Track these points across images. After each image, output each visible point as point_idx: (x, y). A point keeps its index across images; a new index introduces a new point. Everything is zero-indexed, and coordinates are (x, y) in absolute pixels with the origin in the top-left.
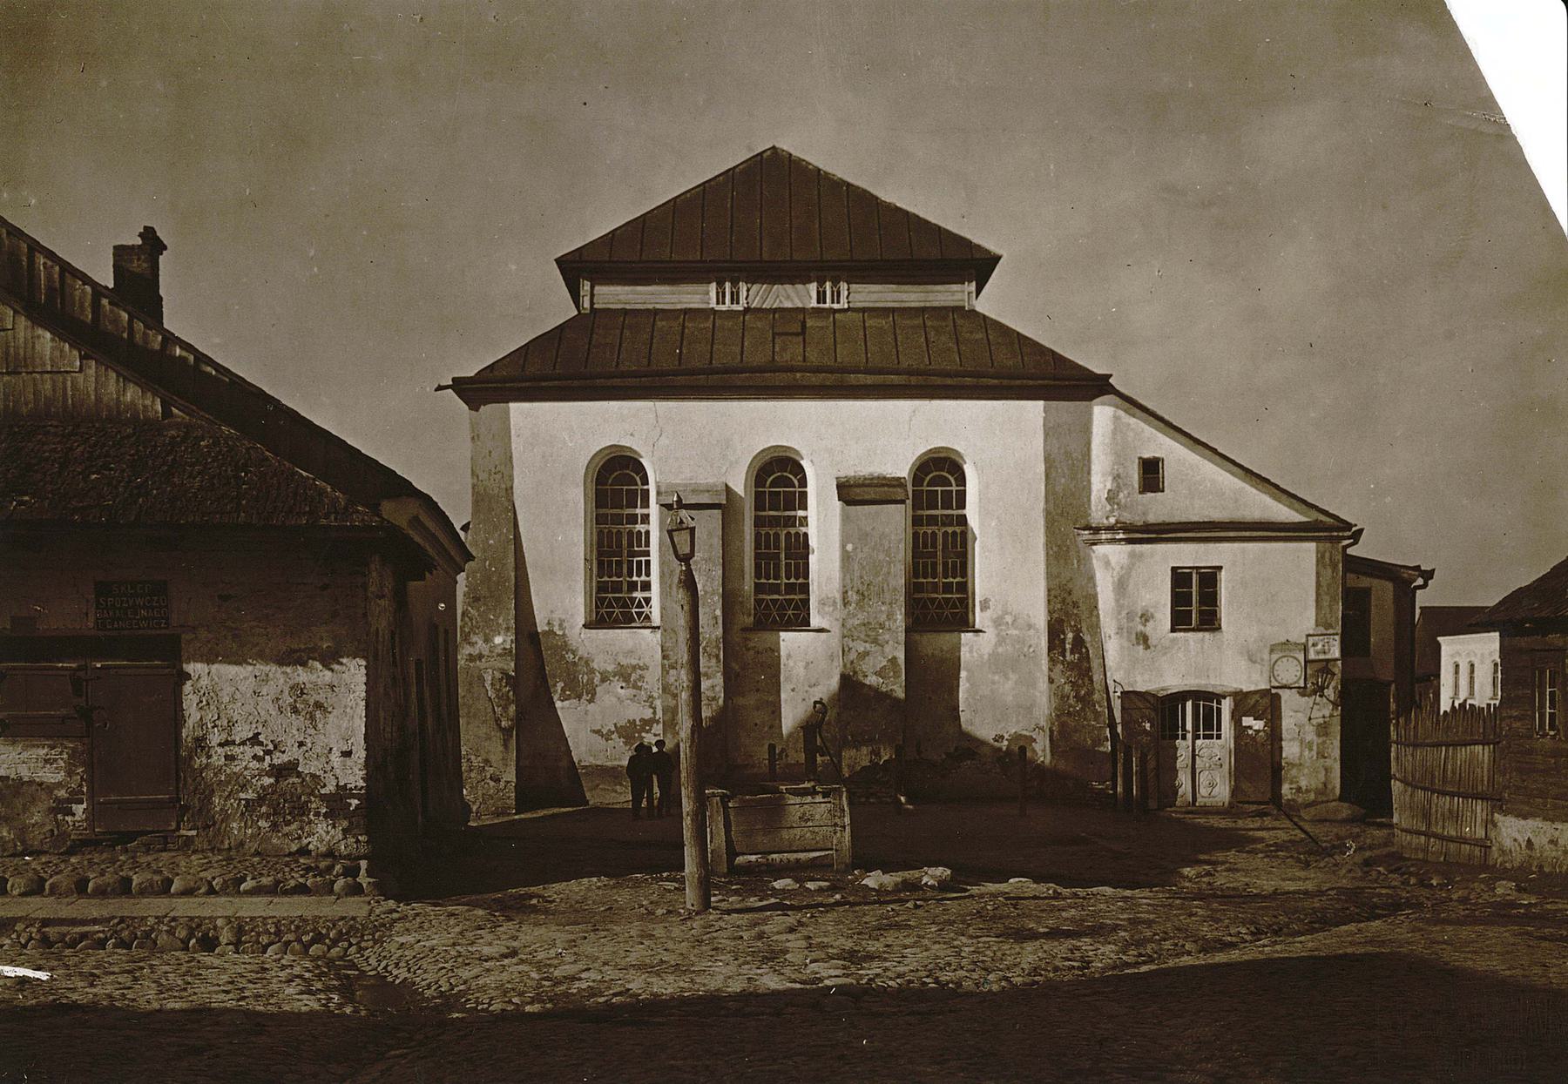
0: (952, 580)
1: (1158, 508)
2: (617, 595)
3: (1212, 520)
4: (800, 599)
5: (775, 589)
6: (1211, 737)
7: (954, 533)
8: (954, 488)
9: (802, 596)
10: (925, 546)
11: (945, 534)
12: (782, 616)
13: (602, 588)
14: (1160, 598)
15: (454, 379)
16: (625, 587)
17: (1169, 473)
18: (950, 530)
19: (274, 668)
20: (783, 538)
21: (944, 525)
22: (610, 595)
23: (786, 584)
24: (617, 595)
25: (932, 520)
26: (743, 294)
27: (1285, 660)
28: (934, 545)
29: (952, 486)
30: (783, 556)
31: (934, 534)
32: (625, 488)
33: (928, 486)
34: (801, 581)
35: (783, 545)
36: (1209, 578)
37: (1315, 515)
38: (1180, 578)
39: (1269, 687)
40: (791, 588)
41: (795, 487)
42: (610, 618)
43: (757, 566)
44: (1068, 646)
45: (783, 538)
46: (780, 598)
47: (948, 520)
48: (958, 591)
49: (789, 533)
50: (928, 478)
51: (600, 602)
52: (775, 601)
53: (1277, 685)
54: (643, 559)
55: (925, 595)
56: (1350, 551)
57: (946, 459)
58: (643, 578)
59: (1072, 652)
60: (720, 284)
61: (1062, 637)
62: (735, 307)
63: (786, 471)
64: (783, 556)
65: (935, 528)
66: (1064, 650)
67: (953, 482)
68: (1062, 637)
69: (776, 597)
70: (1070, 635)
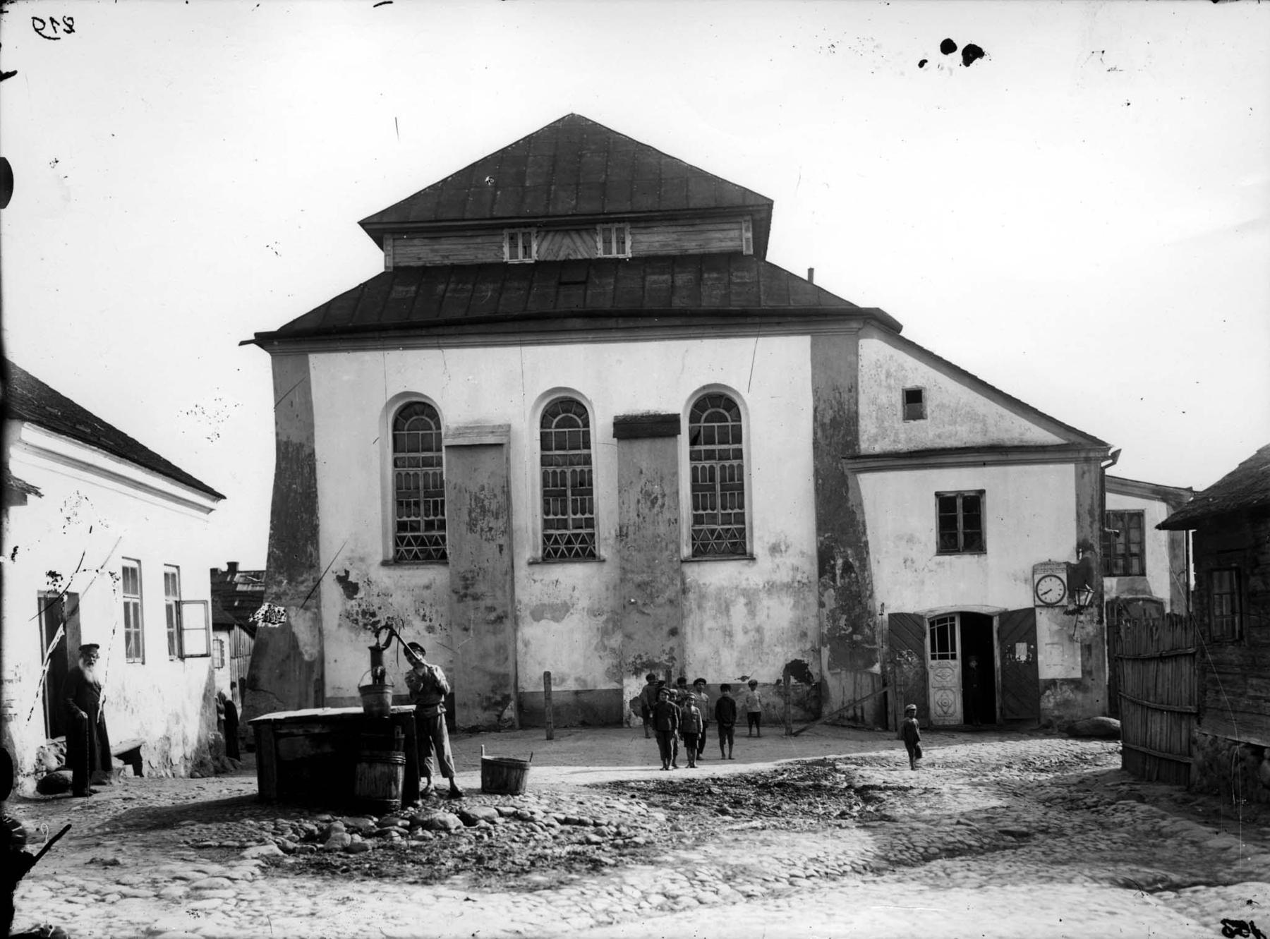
0: (730, 511)
1: (925, 433)
2: (416, 534)
3: (995, 442)
4: (573, 534)
5: (713, 519)
6: (946, 657)
7: (732, 466)
8: (730, 424)
9: (589, 531)
10: (732, 479)
11: (723, 468)
12: (570, 550)
13: (401, 526)
14: (926, 524)
15: (256, 334)
16: (422, 526)
17: (930, 405)
18: (727, 463)
19: (546, 602)
20: (569, 476)
21: (720, 459)
22: (410, 534)
23: (573, 519)
24: (416, 534)
25: (710, 455)
26: (534, 247)
27: (1048, 579)
28: (712, 479)
29: (727, 421)
30: (569, 493)
31: (712, 468)
32: (421, 432)
33: (557, 427)
34: (737, 511)
35: (569, 483)
36: (973, 503)
37: (1073, 438)
38: (946, 503)
39: (1032, 606)
40: (727, 519)
41: (579, 427)
42: (584, 553)
43: (695, 498)
44: (838, 572)
45: (569, 476)
46: (568, 532)
47: (724, 456)
48: (737, 522)
49: (574, 471)
50: (705, 415)
51: (399, 541)
52: (713, 531)
53: (1041, 604)
54: (439, 499)
55: (704, 527)
56: (1108, 472)
57: (721, 396)
58: (440, 517)
59: (842, 577)
60: (513, 238)
61: (832, 562)
62: (528, 261)
63: (719, 407)
64: (569, 493)
65: (712, 462)
66: (834, 575)
67: (729, 419)
68: (832, 562)
69: (564, 532)
70: (840, 562)
